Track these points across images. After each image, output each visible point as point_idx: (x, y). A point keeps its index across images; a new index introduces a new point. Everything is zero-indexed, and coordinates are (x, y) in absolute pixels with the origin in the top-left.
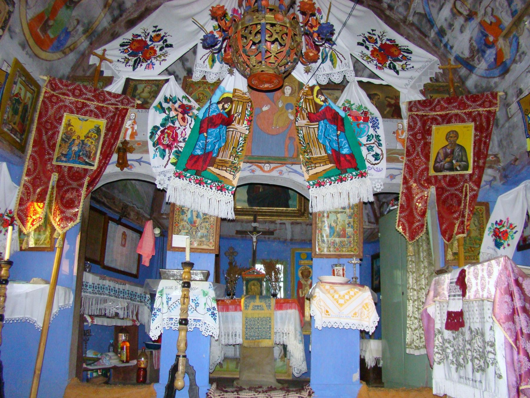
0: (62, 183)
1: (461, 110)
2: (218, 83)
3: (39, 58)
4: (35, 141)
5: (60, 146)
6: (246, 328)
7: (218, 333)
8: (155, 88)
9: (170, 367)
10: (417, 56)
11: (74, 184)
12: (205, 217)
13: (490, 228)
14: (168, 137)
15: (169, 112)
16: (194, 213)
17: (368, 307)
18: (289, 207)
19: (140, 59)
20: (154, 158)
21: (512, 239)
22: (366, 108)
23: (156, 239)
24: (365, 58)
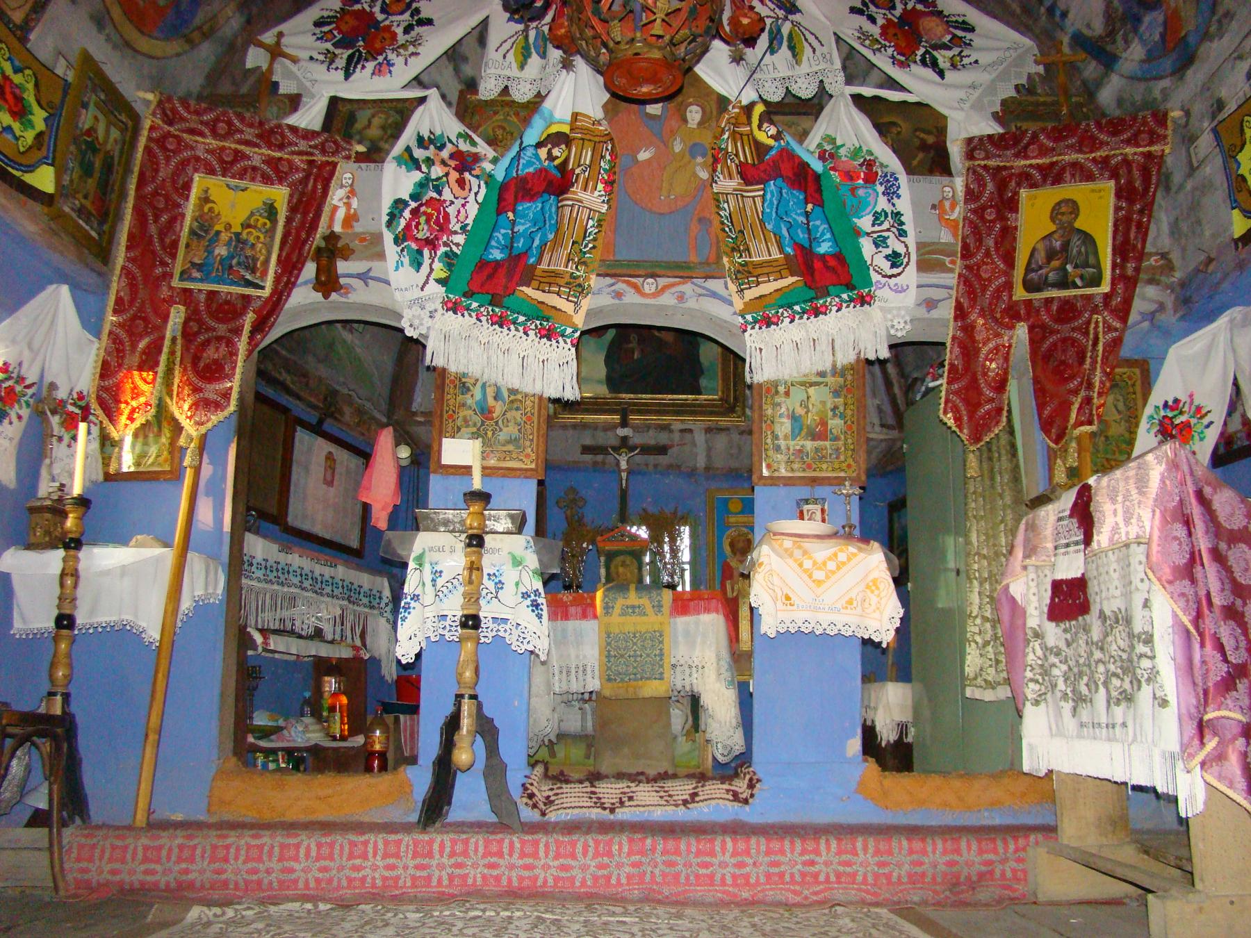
0: (194, 326)
1: (1085, 153)
2: (536, 103)
3: (136, 51)
4: (131, 237)
5: (187, 246)
6: (608, 656)
7: (546, 646)
8: (395, 117)
9: (441, 721)
10: (987, 37)
11: (222, 329)
12: (512, 397)
13: (1152, 417)
14: (428, 221)
15: (429, 168)
16: (488, 390)
17: (878, 588)
18: (700, 393)
19: (360, 53)
20: (397, 269)
21: (1201, 439)
22: (870, 153)
23: (402, 471)
24: (867, 42)
